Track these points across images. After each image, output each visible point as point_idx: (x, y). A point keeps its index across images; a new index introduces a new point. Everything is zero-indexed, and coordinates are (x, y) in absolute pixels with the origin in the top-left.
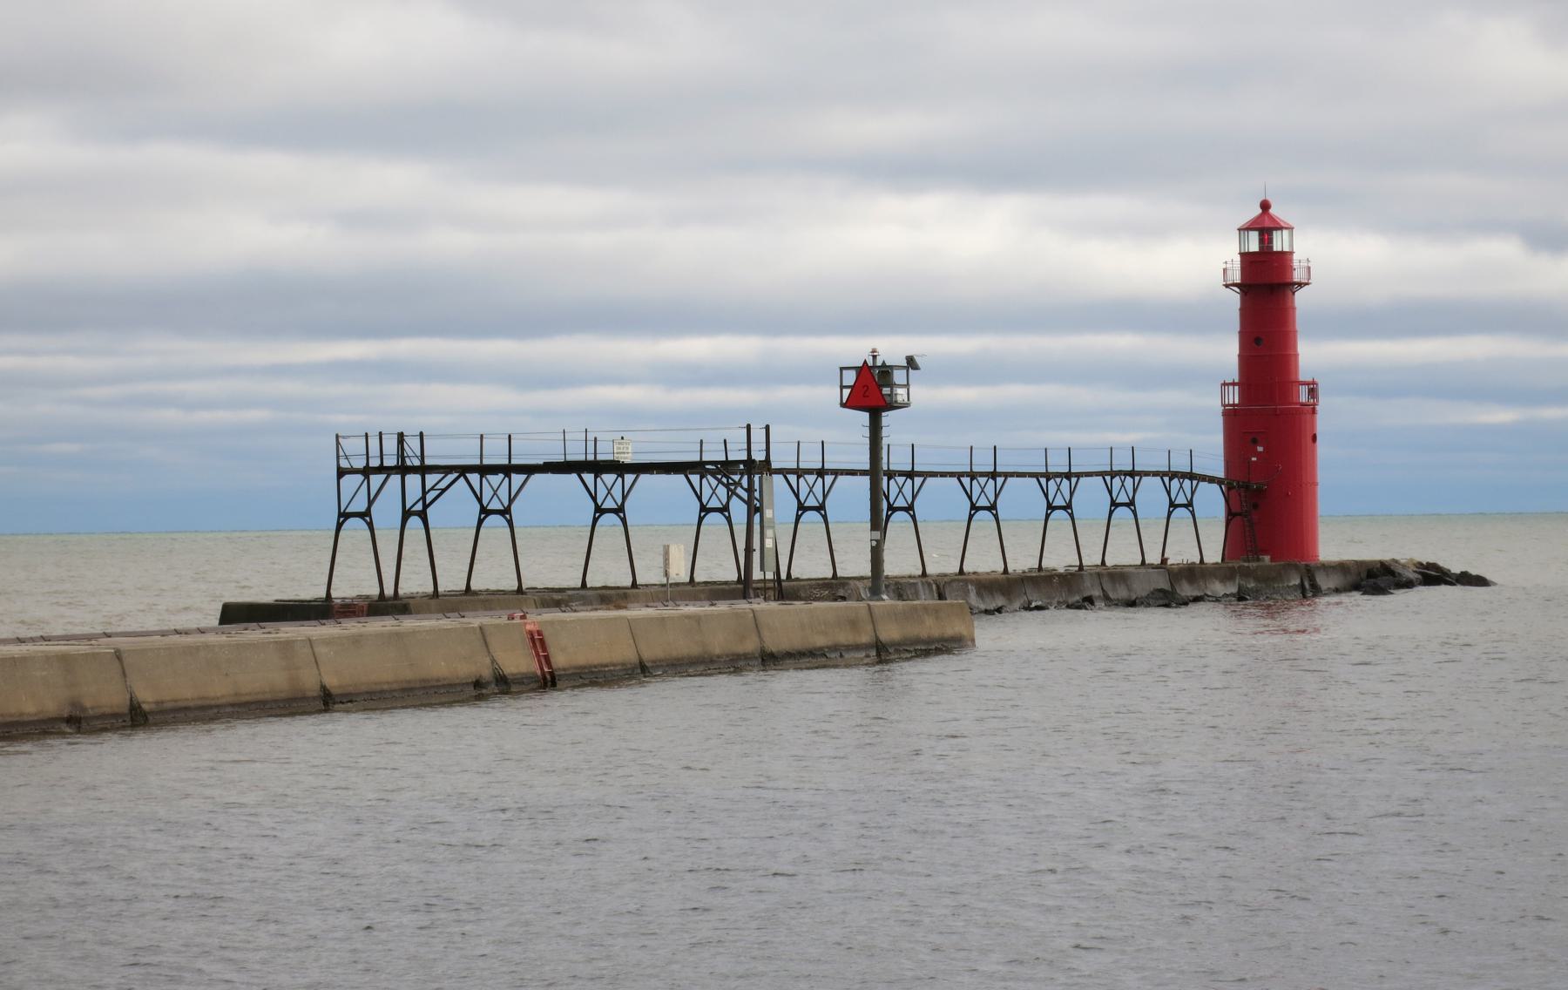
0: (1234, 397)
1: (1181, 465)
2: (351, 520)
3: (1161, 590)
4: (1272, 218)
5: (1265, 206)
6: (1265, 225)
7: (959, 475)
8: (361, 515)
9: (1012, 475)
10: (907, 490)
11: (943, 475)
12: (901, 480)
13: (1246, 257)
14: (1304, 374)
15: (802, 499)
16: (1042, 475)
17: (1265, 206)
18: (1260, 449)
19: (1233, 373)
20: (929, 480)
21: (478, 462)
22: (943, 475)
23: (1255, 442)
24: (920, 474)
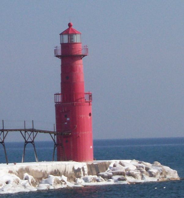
0: (59, 99)
1: (29, 126)
2: (28, 144)
3: (64, 175)
4: (73, 30)
5: (70, 25)
6: (69, 32)
7: (20, 130)
8: (31, 142)
9: (40, 131)
10: (32, 136)
11: (45, 132)
12: (29, 132)
13: (63, 45)
14: (86, 91)
15: (26, 140)
16: (23, 130)
17: (70, 25)
18: (68, 119)
19: (59, 91)
20: (9, 132)
21: (24, 128)
22: (45, 132)
23: (66, 117)
24: (6, 130)
